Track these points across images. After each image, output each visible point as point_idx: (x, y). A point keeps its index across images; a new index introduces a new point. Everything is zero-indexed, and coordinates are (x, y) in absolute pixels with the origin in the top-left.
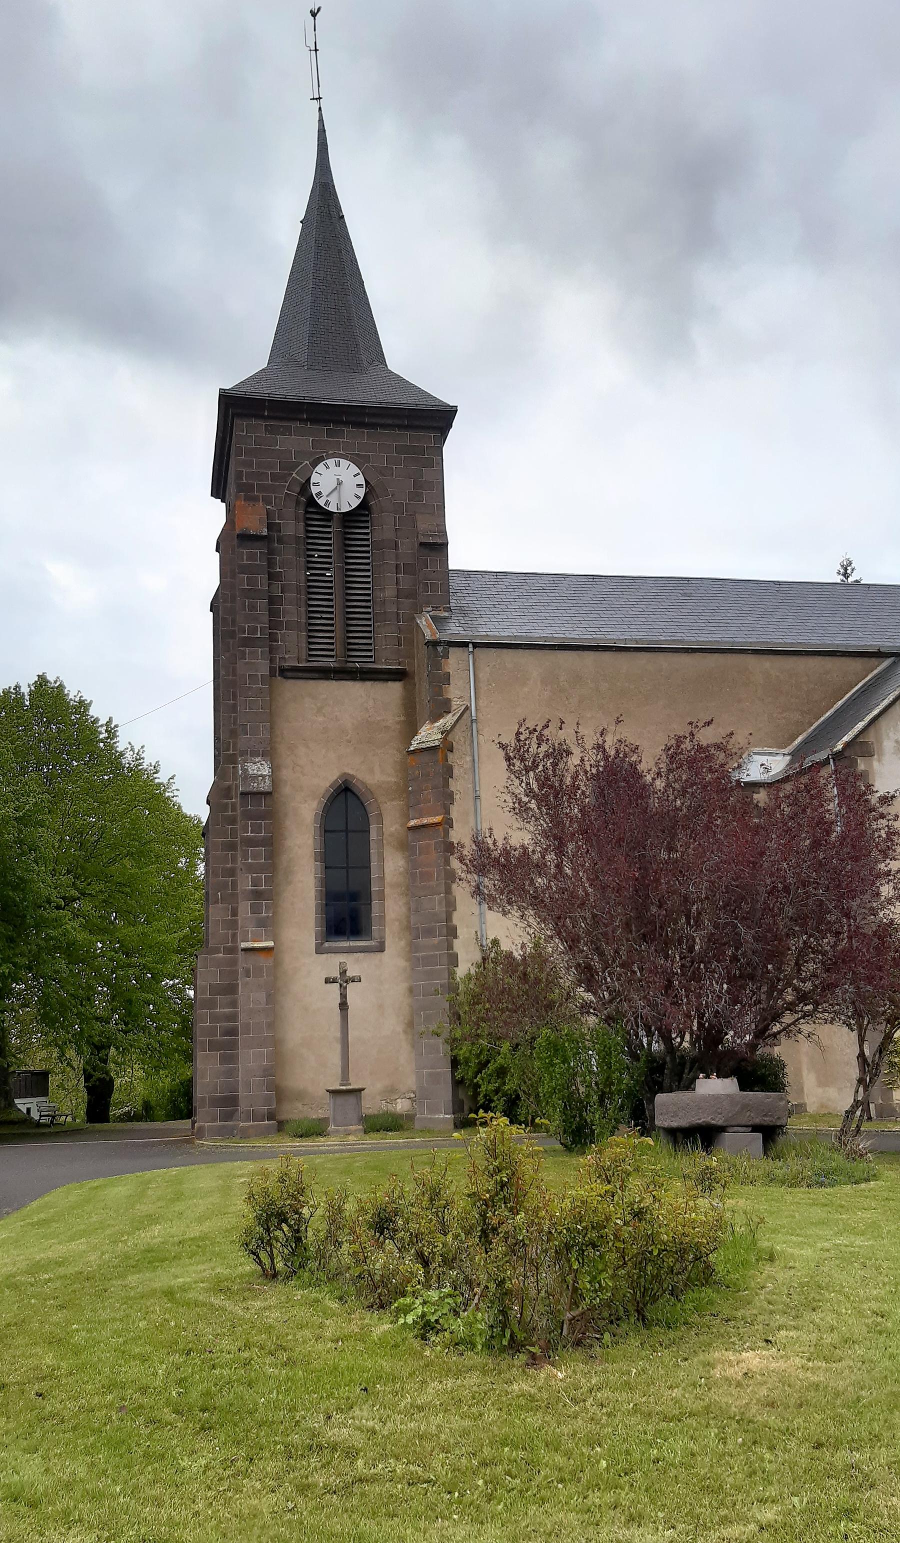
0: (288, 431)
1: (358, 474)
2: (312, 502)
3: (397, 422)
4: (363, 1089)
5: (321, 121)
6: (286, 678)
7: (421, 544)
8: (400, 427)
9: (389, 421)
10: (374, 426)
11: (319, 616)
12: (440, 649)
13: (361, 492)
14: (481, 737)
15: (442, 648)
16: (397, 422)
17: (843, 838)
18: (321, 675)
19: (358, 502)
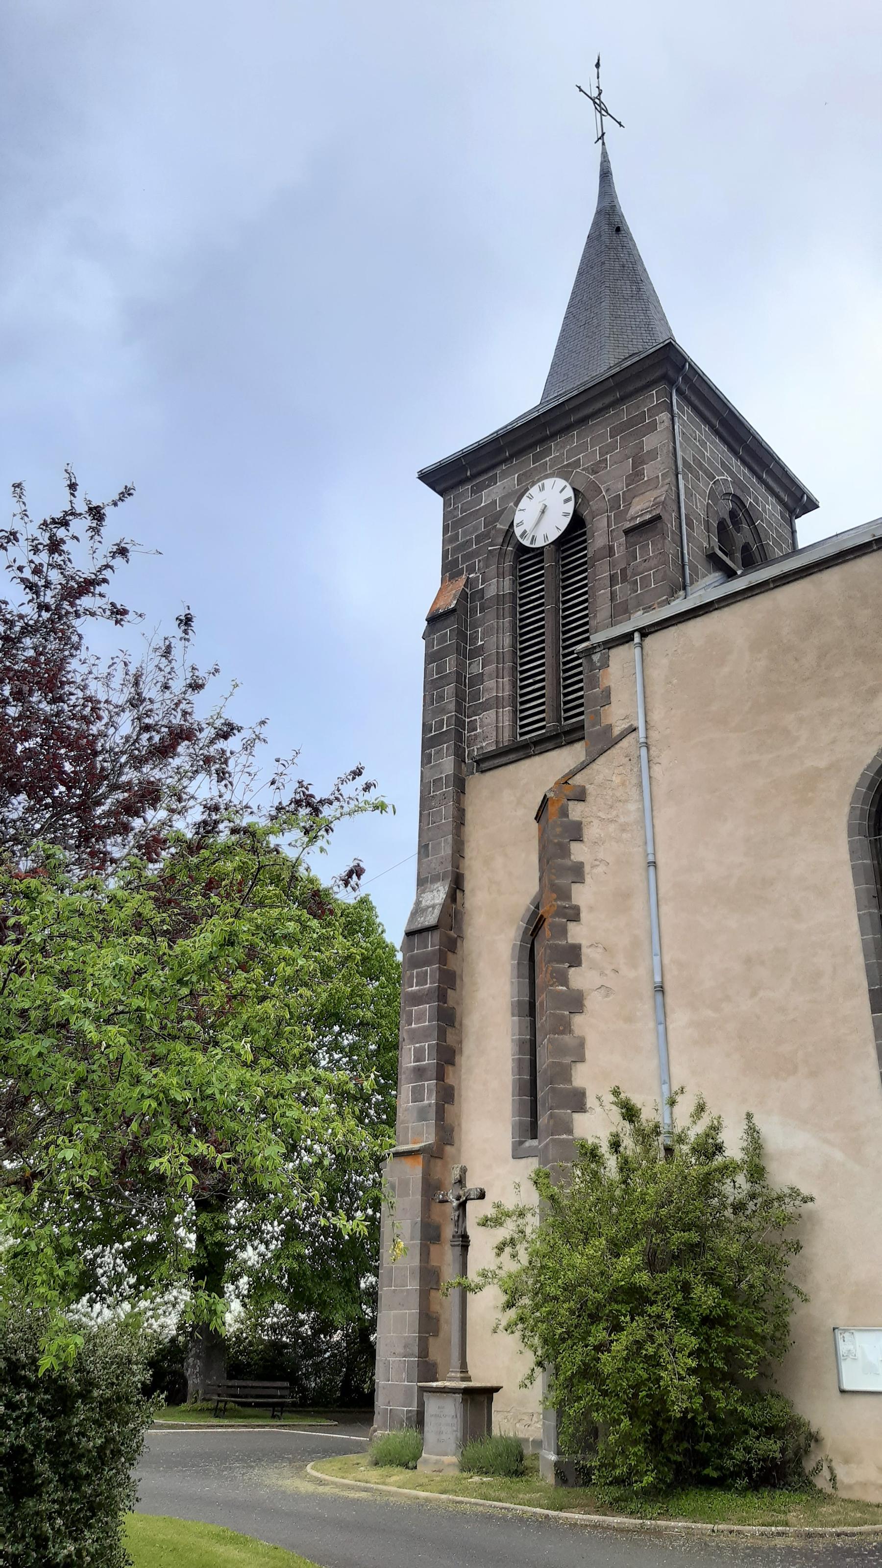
0: (493, 480)
1: (565, 487)
2: (522, 550)
3: (607, 400)
4: (497, 1389)
5: (606, 175)
6: (482, 772)
7: (627, 532)
8: (612, 405)
9: (599, 405)
10: (584, 420)
11: (531, 681)
12: (596, 658)
13: (570, 508)
14: (656, 769)
15: (599, 655)
16: (607, 400)
17: (371, 1265)
18: (521, 754)
19: (567, 520)
